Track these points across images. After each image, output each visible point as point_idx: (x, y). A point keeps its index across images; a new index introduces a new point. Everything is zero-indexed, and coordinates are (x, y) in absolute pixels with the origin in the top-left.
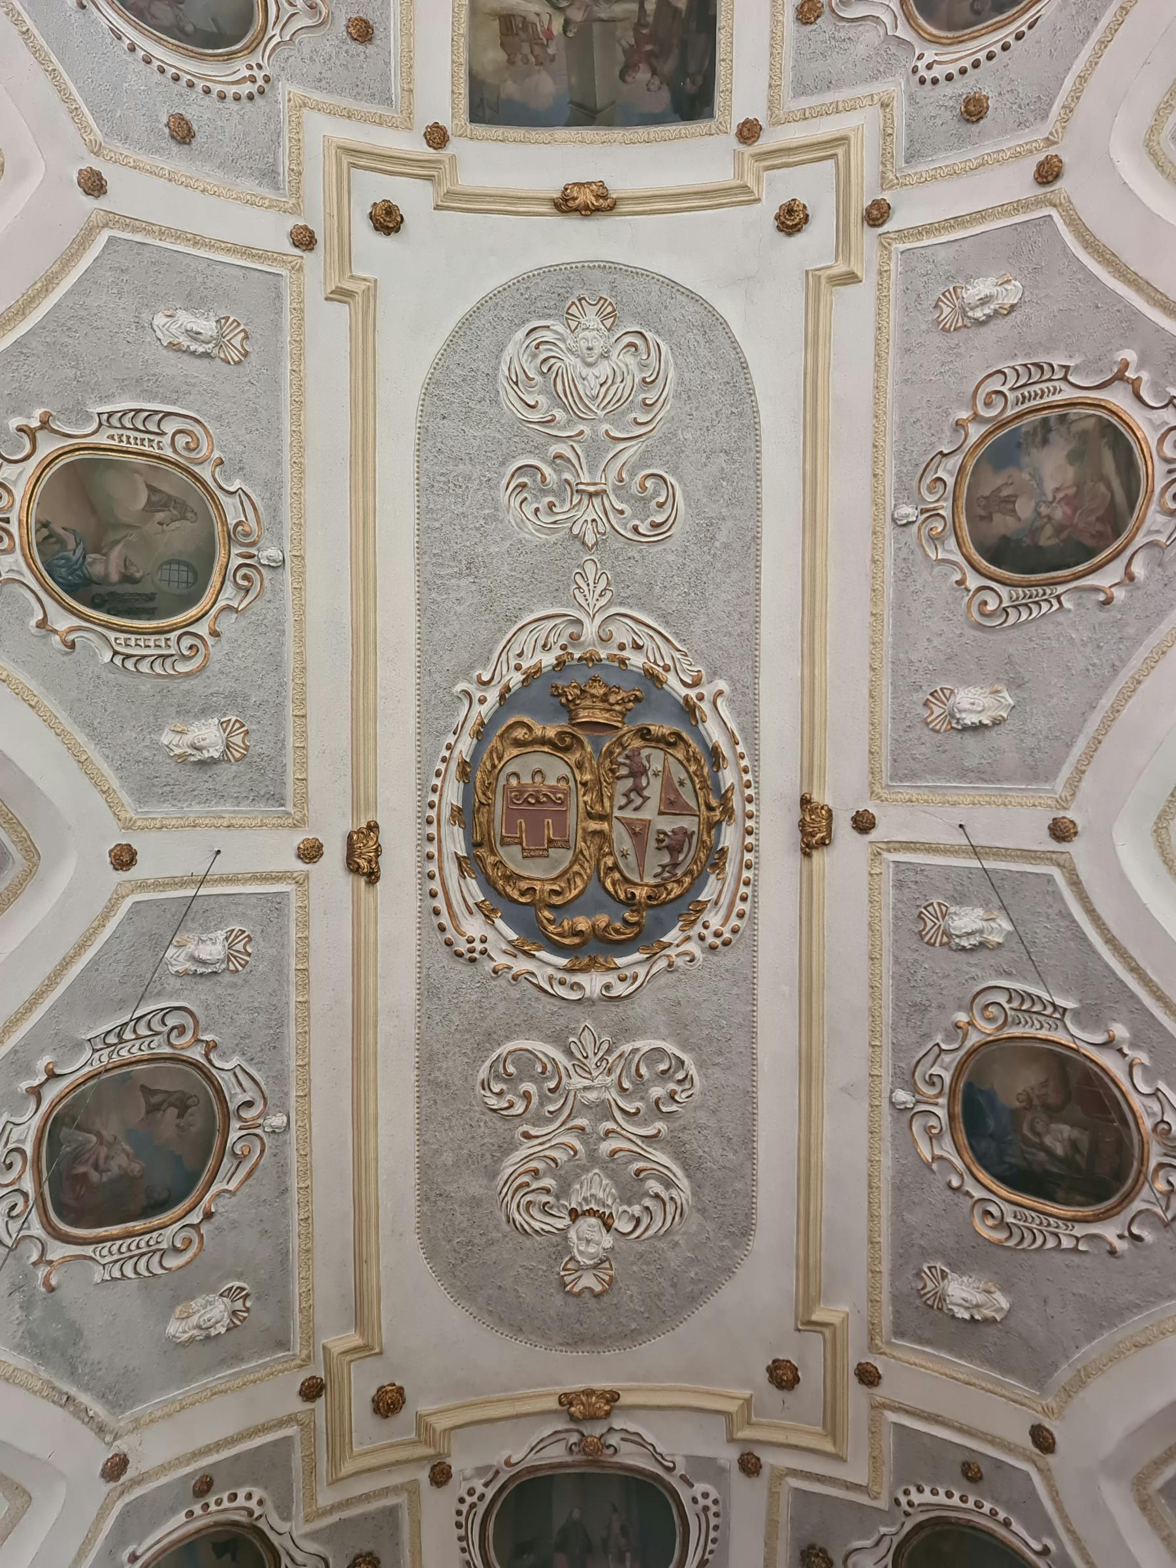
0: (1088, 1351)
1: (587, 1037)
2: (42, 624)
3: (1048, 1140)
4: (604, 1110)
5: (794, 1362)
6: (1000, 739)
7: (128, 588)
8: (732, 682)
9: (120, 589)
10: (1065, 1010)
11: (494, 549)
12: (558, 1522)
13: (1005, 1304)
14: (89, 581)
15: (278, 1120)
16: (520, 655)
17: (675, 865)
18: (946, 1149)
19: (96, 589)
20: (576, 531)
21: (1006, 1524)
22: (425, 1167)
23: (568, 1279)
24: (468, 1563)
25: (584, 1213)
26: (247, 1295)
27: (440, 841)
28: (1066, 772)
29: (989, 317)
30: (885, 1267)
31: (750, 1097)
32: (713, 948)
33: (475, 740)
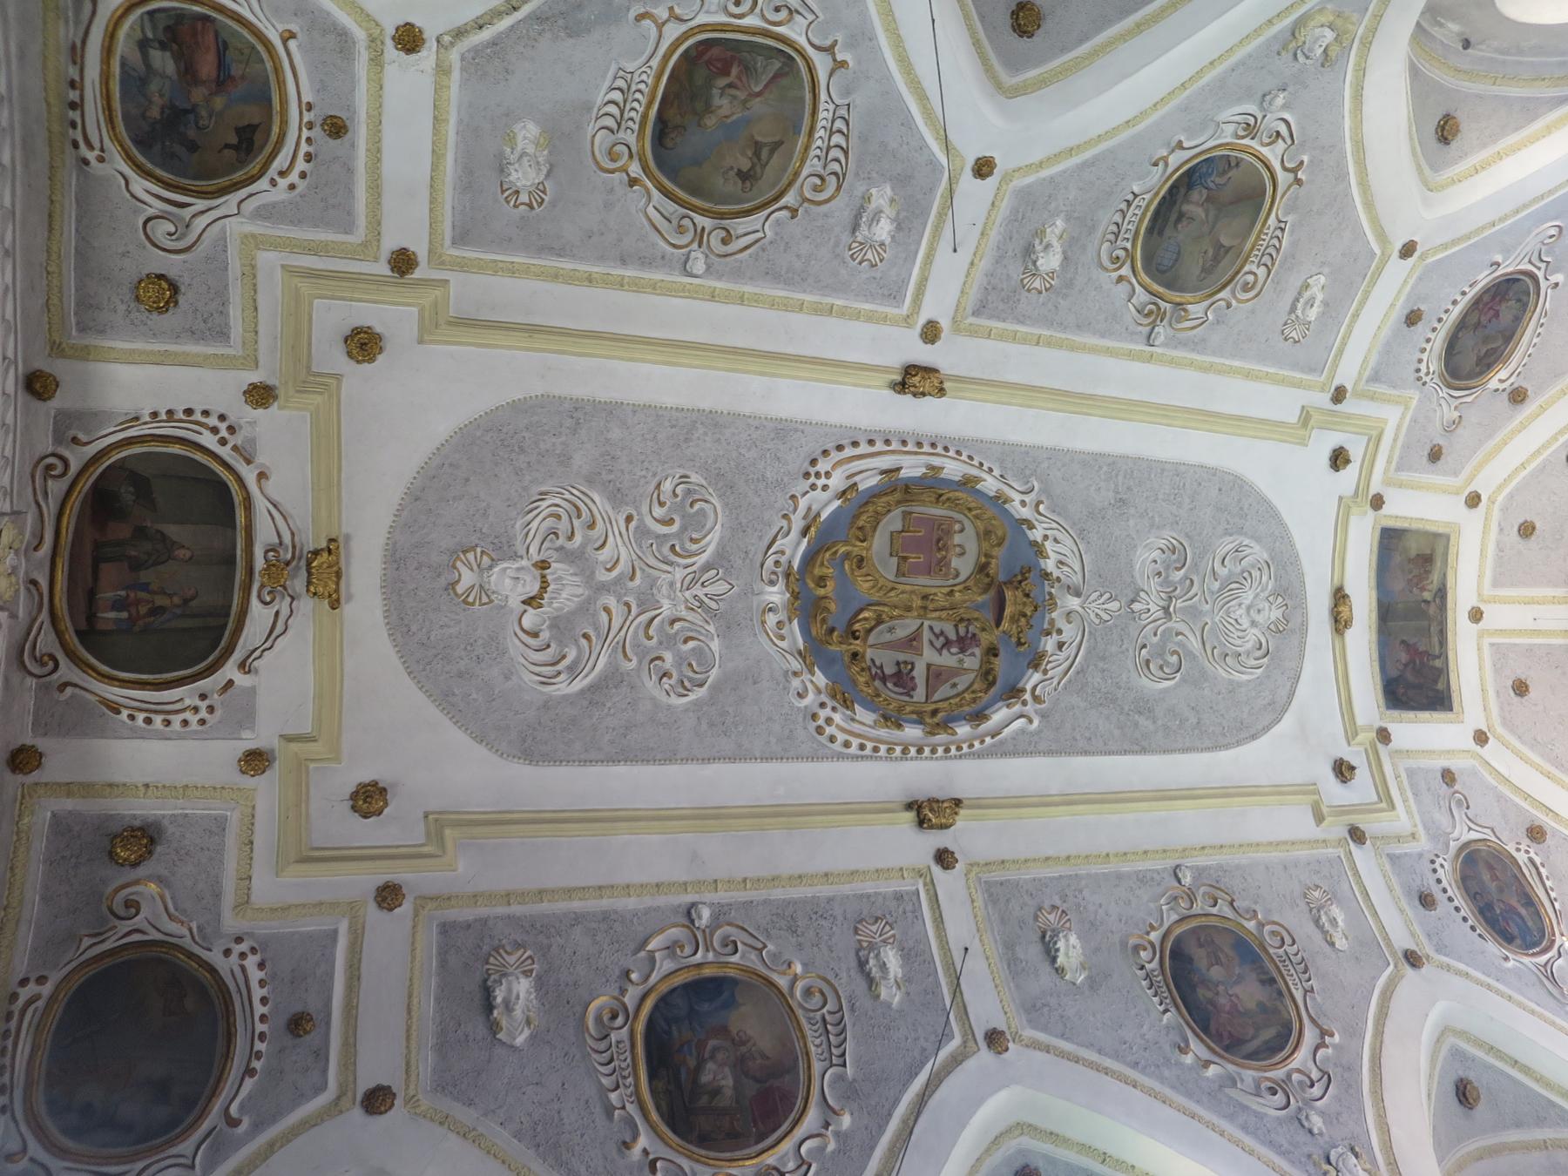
0: (503, 1138)
1: (721, 587)
2: (1180, 146)
3: (710, 1066)
4: (647, 602)
5: (386, 811)
6: (1046, 975)
7: (1174, 217)
8: (1039, 732)
9: (1176, 209)
10: (844, 1065)
11: (1131, 523)
12: (172, 530)
13: (520, 1040)
14: (1190, 187)
15: (699, 266)
16: (1056, 540)
17: (884, 679)
18: (665, 966)
19: (1183, 191)
20: (1142, 594)
21: (250, 1072)
22: (611, 410)
23: (470, 556)
24: (137, 419)
25: (543, 576)
26: (532, 207)
27: (916, 453)
28: (1042, 1037)
29: (868, 974)
30: (516, 909)
31: (670, 758)
32: (814, 717)
33: (992, 494)
